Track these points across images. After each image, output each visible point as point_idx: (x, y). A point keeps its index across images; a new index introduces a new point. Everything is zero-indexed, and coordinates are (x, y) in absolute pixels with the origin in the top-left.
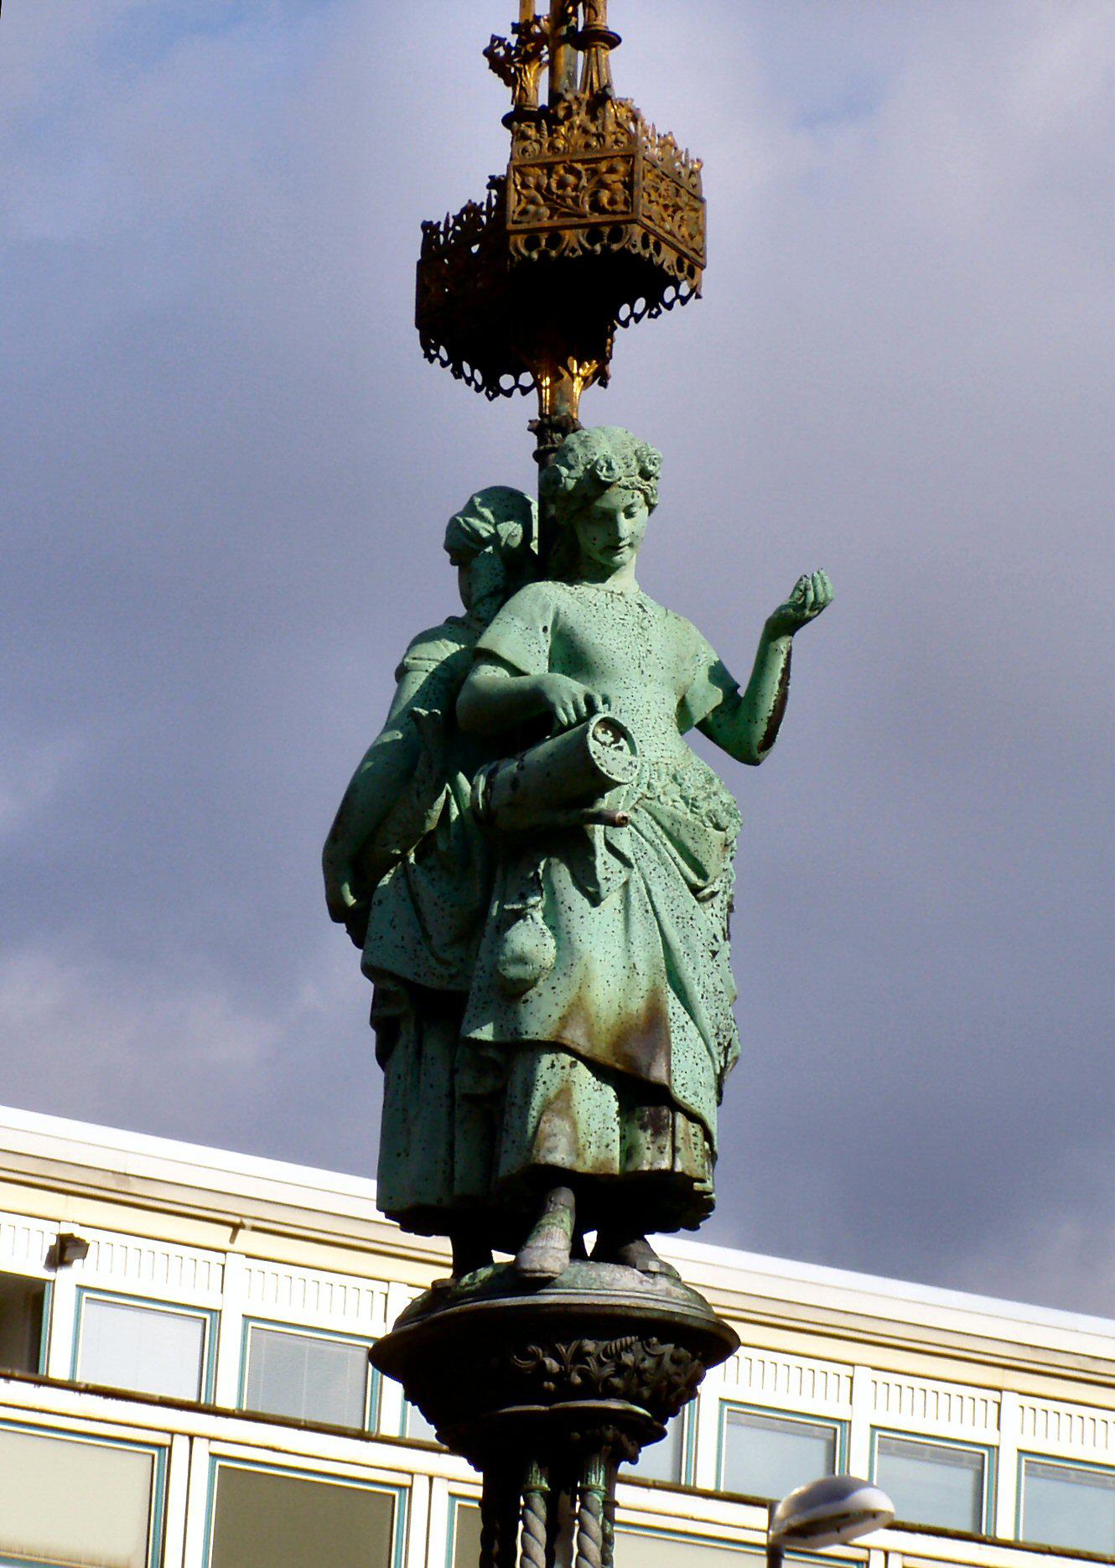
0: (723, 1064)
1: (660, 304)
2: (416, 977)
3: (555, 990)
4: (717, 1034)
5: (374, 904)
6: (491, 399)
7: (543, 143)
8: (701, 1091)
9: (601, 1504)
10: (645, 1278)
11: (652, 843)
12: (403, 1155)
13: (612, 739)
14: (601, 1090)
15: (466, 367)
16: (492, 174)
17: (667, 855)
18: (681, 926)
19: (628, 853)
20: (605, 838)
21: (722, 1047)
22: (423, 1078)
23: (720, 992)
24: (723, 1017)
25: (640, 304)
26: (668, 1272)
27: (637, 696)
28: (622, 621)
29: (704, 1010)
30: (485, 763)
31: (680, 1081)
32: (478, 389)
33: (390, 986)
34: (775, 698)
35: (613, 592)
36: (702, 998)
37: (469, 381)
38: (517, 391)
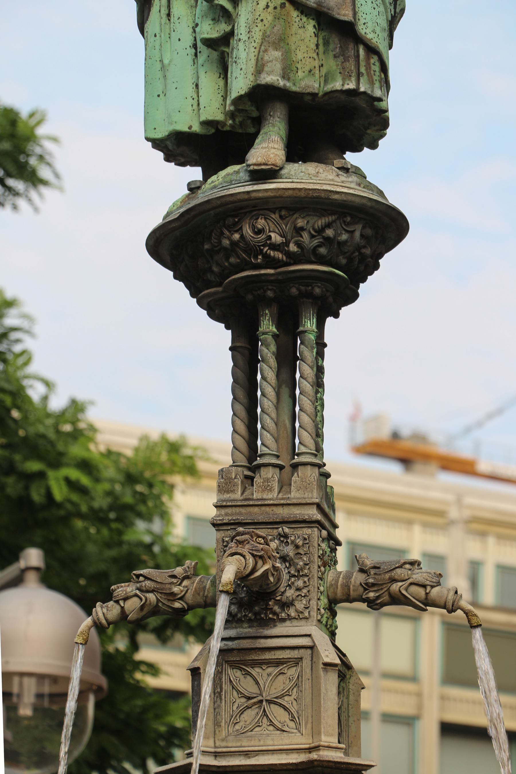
7: (399, 586)
9: (315, 342)
10: (340, 173)
14: (304, 27)
22: (173, 33)
26: (358, 172)
30: (278, 349)
31: (362, 21)
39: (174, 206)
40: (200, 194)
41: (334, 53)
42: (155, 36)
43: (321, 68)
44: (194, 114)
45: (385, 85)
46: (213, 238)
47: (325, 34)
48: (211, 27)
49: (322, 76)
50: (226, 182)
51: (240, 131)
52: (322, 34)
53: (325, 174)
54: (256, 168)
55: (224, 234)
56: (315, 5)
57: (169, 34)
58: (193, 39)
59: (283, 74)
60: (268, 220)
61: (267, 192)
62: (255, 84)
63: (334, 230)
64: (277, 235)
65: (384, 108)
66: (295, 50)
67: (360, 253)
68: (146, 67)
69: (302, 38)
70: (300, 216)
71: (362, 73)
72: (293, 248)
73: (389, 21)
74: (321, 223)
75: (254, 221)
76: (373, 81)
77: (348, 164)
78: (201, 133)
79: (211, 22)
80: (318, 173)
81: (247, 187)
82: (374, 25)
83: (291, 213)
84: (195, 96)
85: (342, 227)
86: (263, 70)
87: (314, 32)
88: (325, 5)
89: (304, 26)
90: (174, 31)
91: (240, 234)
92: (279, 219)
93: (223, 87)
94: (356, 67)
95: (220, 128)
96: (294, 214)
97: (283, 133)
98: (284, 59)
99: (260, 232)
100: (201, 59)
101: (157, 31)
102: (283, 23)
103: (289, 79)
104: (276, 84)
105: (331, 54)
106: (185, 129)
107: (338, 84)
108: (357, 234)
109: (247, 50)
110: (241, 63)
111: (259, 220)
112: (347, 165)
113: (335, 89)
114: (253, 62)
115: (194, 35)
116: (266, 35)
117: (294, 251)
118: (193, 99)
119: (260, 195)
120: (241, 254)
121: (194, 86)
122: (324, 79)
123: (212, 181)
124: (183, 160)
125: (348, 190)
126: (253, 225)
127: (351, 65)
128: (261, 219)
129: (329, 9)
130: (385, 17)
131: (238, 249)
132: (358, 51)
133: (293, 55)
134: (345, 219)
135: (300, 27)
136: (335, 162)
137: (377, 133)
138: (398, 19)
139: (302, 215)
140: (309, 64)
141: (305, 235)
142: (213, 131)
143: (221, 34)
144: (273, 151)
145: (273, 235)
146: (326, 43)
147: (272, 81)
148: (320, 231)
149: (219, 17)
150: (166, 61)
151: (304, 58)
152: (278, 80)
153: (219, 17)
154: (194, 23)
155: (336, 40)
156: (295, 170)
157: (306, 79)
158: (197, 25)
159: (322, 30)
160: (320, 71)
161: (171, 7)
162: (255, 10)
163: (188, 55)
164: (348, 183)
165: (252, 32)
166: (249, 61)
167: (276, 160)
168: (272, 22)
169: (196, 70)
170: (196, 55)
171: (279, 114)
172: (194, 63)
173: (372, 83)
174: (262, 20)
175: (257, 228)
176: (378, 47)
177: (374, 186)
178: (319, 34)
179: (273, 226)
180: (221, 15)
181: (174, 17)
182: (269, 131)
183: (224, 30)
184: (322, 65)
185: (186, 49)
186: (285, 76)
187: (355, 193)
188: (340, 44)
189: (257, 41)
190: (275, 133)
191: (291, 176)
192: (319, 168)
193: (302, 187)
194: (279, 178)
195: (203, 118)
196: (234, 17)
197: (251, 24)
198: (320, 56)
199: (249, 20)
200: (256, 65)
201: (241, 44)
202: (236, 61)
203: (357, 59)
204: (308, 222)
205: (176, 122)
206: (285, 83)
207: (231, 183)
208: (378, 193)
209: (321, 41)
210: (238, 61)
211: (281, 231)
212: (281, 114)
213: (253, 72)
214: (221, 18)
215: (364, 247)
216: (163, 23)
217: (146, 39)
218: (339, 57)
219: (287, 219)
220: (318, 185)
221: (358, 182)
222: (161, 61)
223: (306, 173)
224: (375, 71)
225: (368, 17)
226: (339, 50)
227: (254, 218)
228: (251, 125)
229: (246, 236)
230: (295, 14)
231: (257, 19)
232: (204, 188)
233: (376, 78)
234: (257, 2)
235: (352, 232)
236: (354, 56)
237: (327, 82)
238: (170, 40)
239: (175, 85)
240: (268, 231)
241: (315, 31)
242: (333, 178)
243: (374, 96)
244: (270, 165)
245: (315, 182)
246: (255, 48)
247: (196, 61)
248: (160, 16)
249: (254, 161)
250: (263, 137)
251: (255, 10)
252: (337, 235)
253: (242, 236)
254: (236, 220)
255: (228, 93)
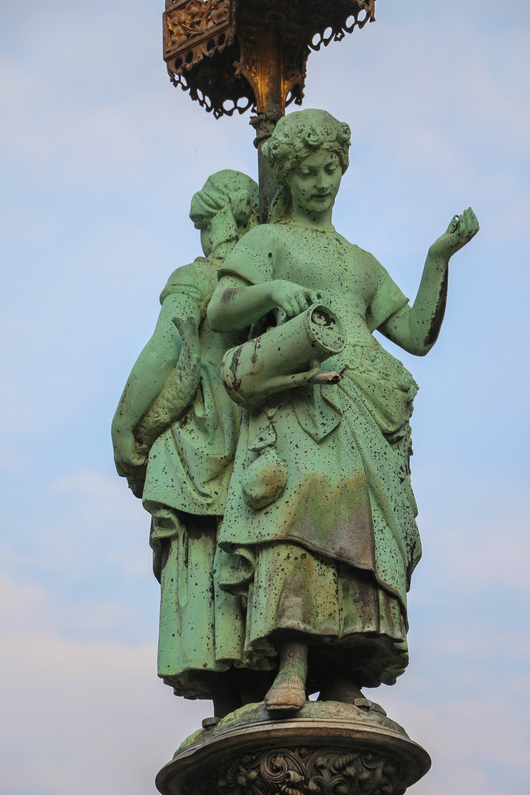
0: (410, 560)
1: (343, 30)
2: (183, 507)
3: (288, 504)
4: (406, 537)
5: (151, 458)
6: (217, 118)
8: (397, 576)
10: (361, 711)
11: (355, 400)
12: (177, 635)
13: (325, 323)
14: (324, 575)
15: (200, 93)
16: (174, 86)
17: (365, 408)
18: (377, 458)
19: (338, 406)
20: (321, 396)
21: (409, 548)
22: (190, 579)
23: (407, 507)
24: (409, 526)
25: (328, 32)
26: (377, 710)
27: (339, 301)
28: (326, 249)
29: (396, 519)
31: (381, 569)
32: (208, 110)
33: (164, 514)
34: (437, 304)
35: (317, 231)
36: (395, 510)
37: (202, 103)
38: (236, 111)
39: (187, 742)
40: (217, 731)
41: (354, 598)
42: (172, 580)
43: (341, 612)
44: (210, 652)
45: (404, 626)
46: (228, 775)
47: (345, 580)
48: (230, 574)
49: (342, 619)
50: (244, 720)
51: (257, 669)
52: (341, 582)
53: (346, 713)
54: (276, 707)
55: (240, 771)
56: (335, 556)
57: (186, 579)
58: (210, 583)
59: (303, 618)
60: (286, 758)
61: (287, 731)
62: (276, 627)
63: (355, 768)
64: (296, 774)
65: (404, 649)
66: (315, 596)
67: (381, 791)
68: (161, 609)
69: (323, 585)
70: (320, 754)
71: (382, 616)
72: (312, 786)
73: (407, 567)
74: (342, 760)
75: (273, 760)
76: (393, 624)
77: (369, 703)
78: (216, 671)
79: (230, 570)
80: (338, 711)
81: (266, 726)
82: (393, 572)
83: (311, 751)
84: (211, 636)
85: (363, 765)
86: (283, 615)
87: (334, 580)
88: (345, 555)
89: (324, 574)
90: (191, 576)
91: (257, 771)
92: (298, 757)
93: (239, 628)
94: (376, 611)
95: (235, 665)
96: (313, 752)
97: (303, 673)
98: (305, 604)
99: (278, 770)
100: (218, 602)
101: (174, 576)
102: (304, 572)
103: (309, 623)
104: (296, 627)
105: (351, 599)
106: (200, 667)
107: (358, 627)
108: (379, 772)
109: (267, 596)
110: (261, 608)
111: (278, 758)
112: (368, 704)
113: (355, 631)
114: (274, 607)
115: (211, 580)
116: (287, 583)
117: (314, 789)
118: (209, 639)
119: (280, 734)
120: (257, 792)
121: (210, 626)
122: (343, 622)
123: (229, 719)
124: (193, 694)
125: (370, 729)
126: (271, 762)
127: (371, 609)
128: (280, 757)
129: (349, 559)
130: (403, 564)
131: (254, 787)
132: (378, 596)
133: (313, 600)
134: (366, 757)
135: (320, 575)
136: (355, 700)
137: (396, 671)
138: (414, 565)
139: (322, 754)
140: (329, 608)
141: (326, 773)
142: (228, 668)
143: (240, 580)
144: (293, 691)
145: (292, 773)
146: (346, 589)
147: (292, 625)
148: (341, 769)
149: (238, 565)
150: (182, 604)
151: (324, 603)
152: (298, 624)
153: (238, 565)
154: (211, 569)
155: (356, 586)
156: (315, 709)
157: (326, 622)
158: (215, 571)
159: (342, 577)
160: (339, 614)
161: (189, 555)
162: (276, 560)
163: (204, 598)
164: (369, 722)
165: (273, 580)
166: (269, 606)
167: (297, 700)
168: (293, 572)
169: (212, 611)
170: (213, 598)
171: (298, 655)
172: (211, 606)
173: (392, 625)
174: (283, 570)
175: (276, 766)
176: (397, 592)
177: (396, 724)
178: (339, 581)
179: (292, 764)
180: (241, 563)
181: (191, 564)
182: (289, 672)
183: (244, 578)
184: (342, 609)
185: (203, 592)
186: (306, 620)
187: (378, 732)
188: (360, 590)
189: (277, 588)
190: (295, 673)
191: (311, 716)
192: (339, 707)
193: (323, 726)
194: (299, 717)
195: (218, 657)
196: (254, 566)
197: (272, 573)
198: (340, 601)
199: (269, 569)
200: (277, 610)
201: (261, 591)
202: (256, 606)
203: (376, 603)
204: (328, 760)
205: (191, 661)
206: (306, 626)
207: (249, 721)
208: (399, 731)
209: (340, 587)
210: (258, 606)
211: (300, 769)
212: (301, 654)
213: (273, 617)
214: (240, 567)
215: (386, 785)
216: (180, 569)
217: (163, 583)
218: (358, 602)
219: (307, 757)
220: (340, 724)
221: (379, 720)
222: (178, 603)
223: (327, 711)
224: (395, 614)
225: (387, 565)
226: (359, 595)
227: (273, 756)
228: (268, 664)
229: (264, 774)
230: (315, 563)
231: (278, 569)
232: (220, 726)
233: (396, 620)
234: (278, 553)
235: (373, 770)
236: (374, 600)
237: (347, 625)
238: (187, 584)
239: (191, 626)
240: (286, 769)
241: (335, 578)
242: (354, 716)
243: (395, 637)
244: (291, 705)
245: (336, 720)
246: (276, 595)
247: (212, 603)
248: (178, 562)
249: (275, 701)
250: (283, 677)
251: (276, 560)
252: (358, 773)
253: (259, 774)
254: (254, 758)
255: (247, 635)
